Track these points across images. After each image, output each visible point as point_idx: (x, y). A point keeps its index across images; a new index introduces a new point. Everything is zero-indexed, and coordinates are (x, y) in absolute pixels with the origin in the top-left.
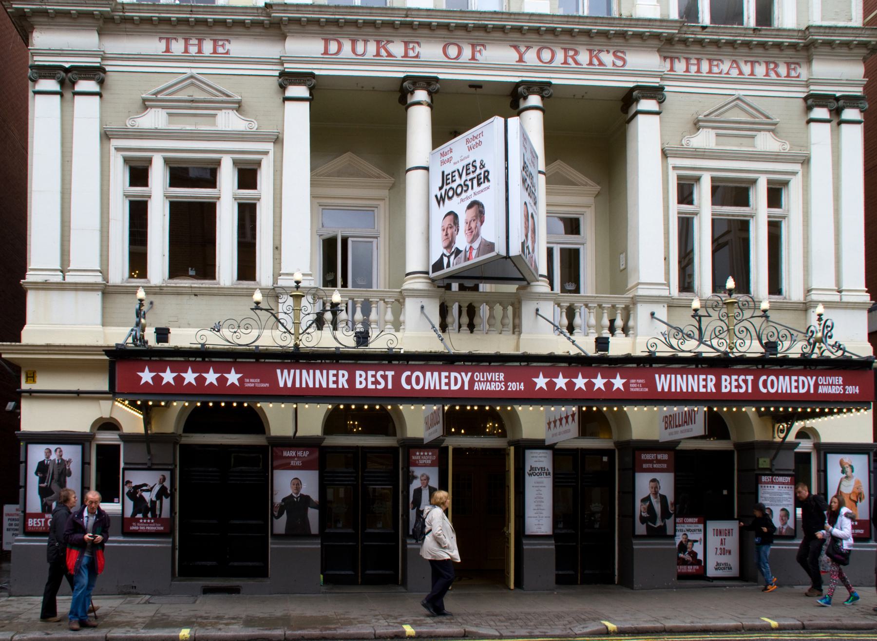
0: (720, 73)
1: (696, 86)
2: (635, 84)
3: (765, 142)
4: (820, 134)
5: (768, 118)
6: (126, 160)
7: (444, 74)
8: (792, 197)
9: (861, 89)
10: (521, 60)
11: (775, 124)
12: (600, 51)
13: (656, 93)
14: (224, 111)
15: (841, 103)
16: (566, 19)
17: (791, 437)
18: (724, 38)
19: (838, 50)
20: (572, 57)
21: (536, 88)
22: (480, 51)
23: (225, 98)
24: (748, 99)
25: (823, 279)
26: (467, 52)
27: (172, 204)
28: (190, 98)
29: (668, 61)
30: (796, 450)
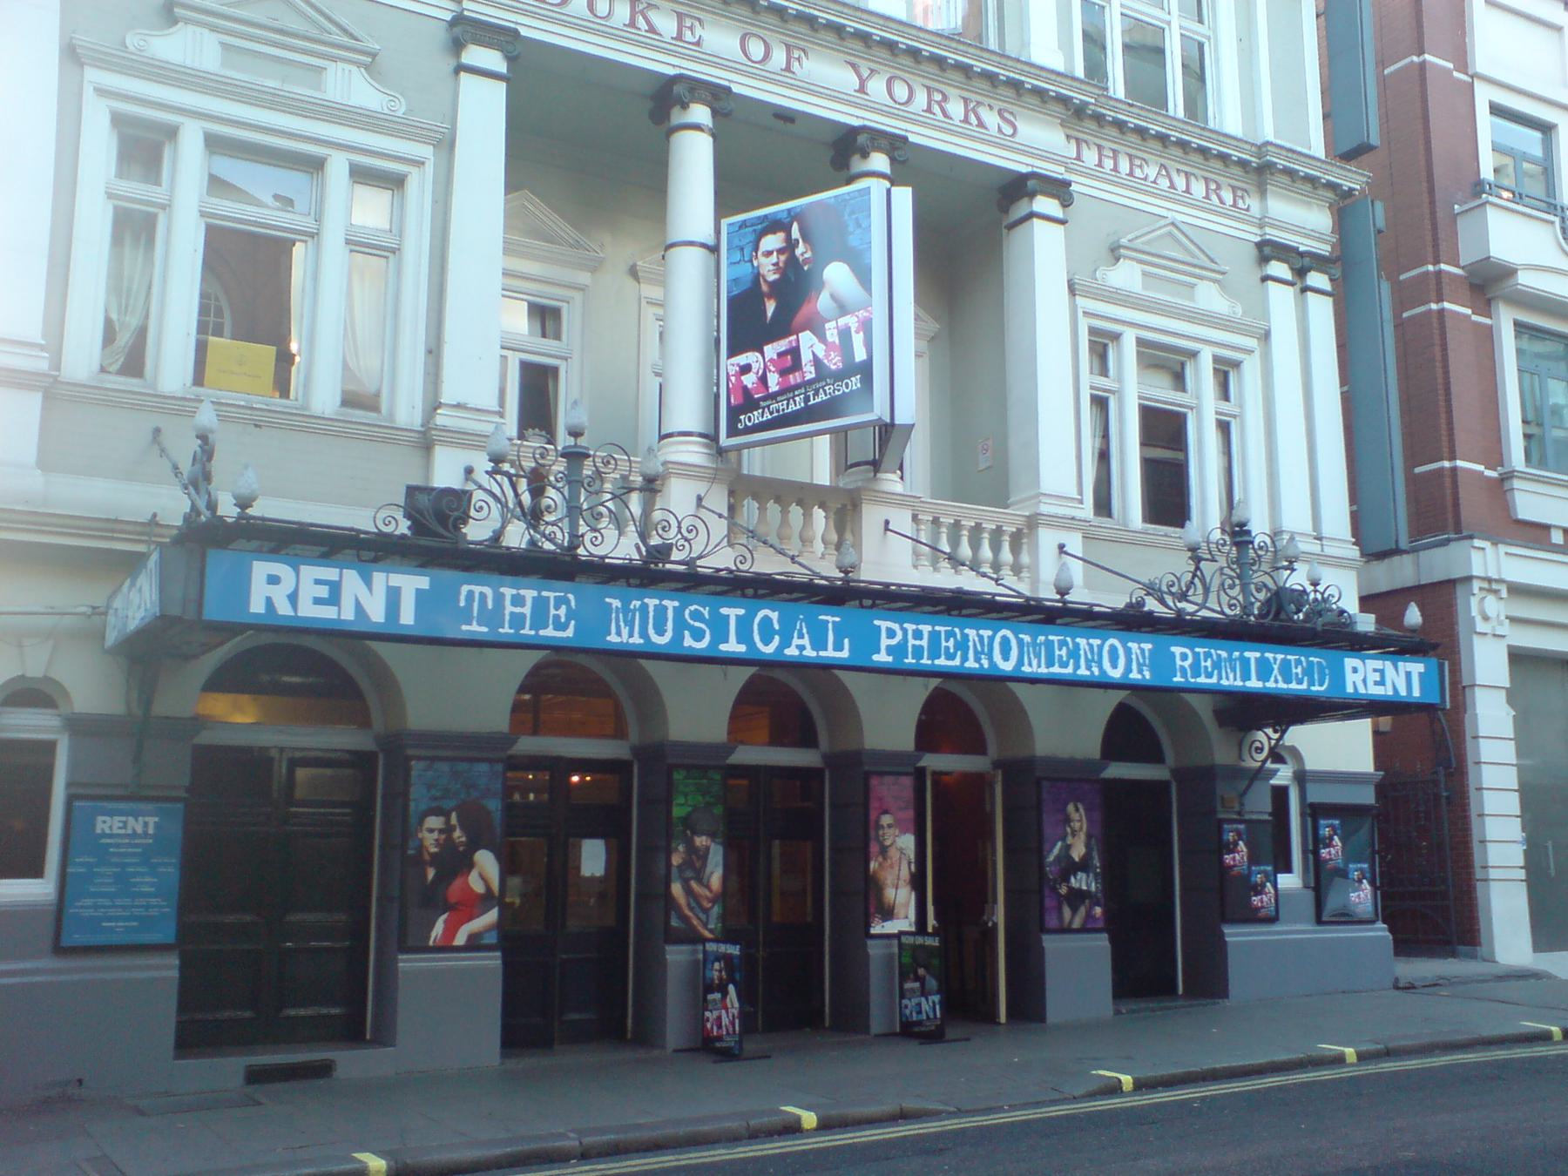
0: (1145, 179)
1: (1114, 187)
2: (1029, 169)
3: (348, 85)
4: (1281, 299)
5: (1212, 261)
6: (118, 120)
7: (744, 87)
8: (1249, 380)
9: (1329, 248)
10: (862, 89)
11: (1223, 273)
12: (979, 103)
13: (1060, 189)
14: (340, 65)
15: (1307, 260)
16: (938, 40)
17: (1253, 762)
18: (1133, 122)
19: (1299, 184)
20: (939, 103)
21: (884, 143)
22: (799, 59)
23: (345, 40)
24: (1182, 226)
25: (1296, 518)
26: (779, 57)
27: (210, 229)
28: (276, 24)
29: (1073, 142)
30: (1272, 782)
